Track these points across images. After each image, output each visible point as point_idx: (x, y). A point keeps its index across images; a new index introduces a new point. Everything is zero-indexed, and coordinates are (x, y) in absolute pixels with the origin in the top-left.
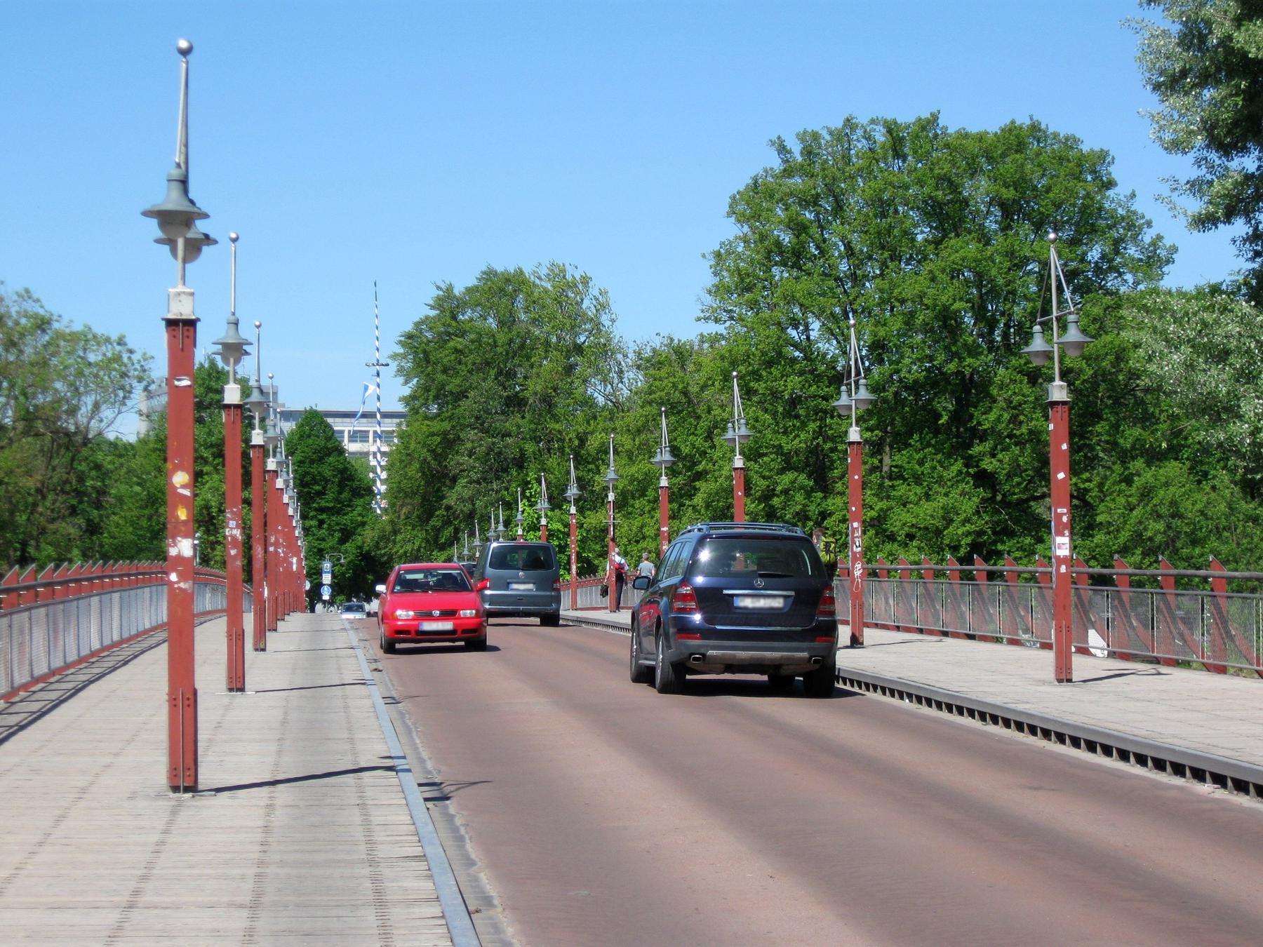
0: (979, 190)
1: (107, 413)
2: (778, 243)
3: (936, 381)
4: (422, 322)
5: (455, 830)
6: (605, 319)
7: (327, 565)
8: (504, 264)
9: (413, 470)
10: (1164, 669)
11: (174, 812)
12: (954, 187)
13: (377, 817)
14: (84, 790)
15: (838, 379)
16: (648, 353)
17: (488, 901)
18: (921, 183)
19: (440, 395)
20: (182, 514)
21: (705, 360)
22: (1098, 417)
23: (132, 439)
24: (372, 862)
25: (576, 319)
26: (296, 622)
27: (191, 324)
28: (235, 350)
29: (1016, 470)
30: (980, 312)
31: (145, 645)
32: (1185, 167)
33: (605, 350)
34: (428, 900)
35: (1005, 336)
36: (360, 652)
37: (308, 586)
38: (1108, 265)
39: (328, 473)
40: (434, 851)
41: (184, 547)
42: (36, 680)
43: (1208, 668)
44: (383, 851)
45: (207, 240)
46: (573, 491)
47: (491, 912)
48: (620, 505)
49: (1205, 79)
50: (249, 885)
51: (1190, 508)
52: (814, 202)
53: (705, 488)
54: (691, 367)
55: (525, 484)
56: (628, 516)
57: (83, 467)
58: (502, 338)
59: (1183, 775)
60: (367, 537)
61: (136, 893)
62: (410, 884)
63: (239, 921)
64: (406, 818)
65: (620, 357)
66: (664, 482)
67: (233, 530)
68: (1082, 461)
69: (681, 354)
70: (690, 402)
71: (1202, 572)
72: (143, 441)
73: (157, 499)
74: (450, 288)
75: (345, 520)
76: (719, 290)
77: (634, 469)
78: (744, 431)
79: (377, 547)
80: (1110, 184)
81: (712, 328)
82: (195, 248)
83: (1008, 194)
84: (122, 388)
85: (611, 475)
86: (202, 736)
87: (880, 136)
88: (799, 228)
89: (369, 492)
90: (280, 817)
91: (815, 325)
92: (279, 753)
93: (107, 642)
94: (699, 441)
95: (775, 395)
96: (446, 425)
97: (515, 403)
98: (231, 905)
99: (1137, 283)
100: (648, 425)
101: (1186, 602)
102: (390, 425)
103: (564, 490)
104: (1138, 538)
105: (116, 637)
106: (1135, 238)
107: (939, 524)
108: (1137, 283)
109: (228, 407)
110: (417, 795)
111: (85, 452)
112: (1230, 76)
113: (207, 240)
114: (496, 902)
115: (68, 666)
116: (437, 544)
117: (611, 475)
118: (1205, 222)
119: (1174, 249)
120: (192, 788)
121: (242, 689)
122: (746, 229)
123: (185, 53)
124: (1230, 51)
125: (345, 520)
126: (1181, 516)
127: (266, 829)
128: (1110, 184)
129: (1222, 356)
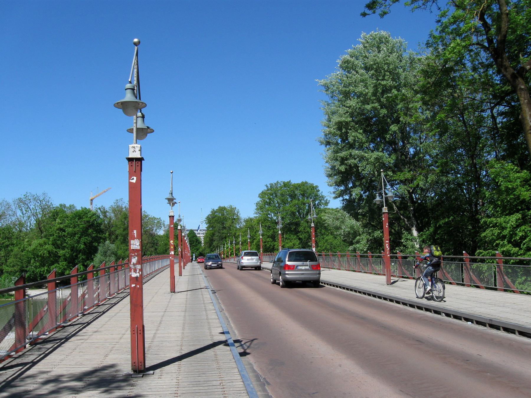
0: (297, 192)
1: (158, 230)
2: (267, 202)
3: (290, 224)
4: (209, 215)
5: (217, 298)
6: (239, 214)
7: (194, 255)
8: (222, 206)
9: (208, 239)
10: (330, 269)
11: (171, 296)
12: (294, 192)
13: (205, 296)
14: (156, 293)
15: (277, 223)
16: (246, 220)
17: (223, 310)
18: (288, 191)
19: (212, 227)
20: (172, 247)
21: (255, 221)
22: (318, 228)
23: (162, 235)
24: (204, 304)
25: (234, 214)
26: (189, 264)
27: (173, 216)
28: (180, 220)
29: (305, 237)
30: (299, 211)
31: (165, 268)
32: (332, 189)
33: (238, 219)
34: (214, 310)
35: (303, 216)
36: (200, 269)
37: (191, 258)
38: (319, 204)
39: (194, 240)
40: (215, 302)
41: (173, 253)
42: (148, 275)
43: (338, 269)
44: (206, 302)
45: (176, 203)
46: (234, 242)
47: (224, 312)
48: (241, 244)
49: (335, 175)
50: (184, 308)
51: (334, 243)
52: (272, 195)
53: (255, 241)
54: (253, 221)
55: (226, 241)
56: (243, 246)
57: (154, 239)
58: (222, 217)
59: (334, 287)
60: (201, 250)
61: (166, 309)
62: (211, 307)
63: (183, 314)
64: (209, 296)
65: (241, 220)
66: (249, 240)
67: (180, 250)
68: (316, 236)
69: (251, 219)
70: (253, 227)
71: (336, 254)
72: (164, 235)
73: (167, 244)
74: (214, 210)
75: (197, 247)
76: (257, 209)
77: (244, 238)
78: (262, 232)
79: (202, 251)
80: (319, 191)
81: (256, 215)
82: (174, 204)
83: (302, 193)
84: (160, 226)
85: (240, 239)
86: (176, 283)
87: (282, 184)
88: (270, 199)
89: (200, 243)
90: (189, 297)
91: (272, 214)
92: (188, 286)
93: (159, 268)
94: (254, 234)
95: (266, 226)
96: (213, 232)
97: (224, 228)
98: (181, 311)
99: (324, 207)
100: (246, 231)
101: (333, 258)
102: (204, 232)
103: (233, 242)
104: (326, 248)
105: (160, 267)
106: (323, 199)
107: (293, 246)
108: (324, 207)
109: (179, 230)
110: (211, 292)
111: (154, 237)
112: (339, 174)
113: (176, 203)
114: (224, 310)
115: (153, 272)
116: (212, 251)
117: (240, 239)
118: (336, 198)
119: (329, 201)
120: (174, 292)
121: (181, 276)
122: (261, 199)
123: (172, 173)
124: (339, 170)
125: (197, 247)
126: (333, 245)
127: (186, 298)
128: (319, 191)
129: (338, 219)
